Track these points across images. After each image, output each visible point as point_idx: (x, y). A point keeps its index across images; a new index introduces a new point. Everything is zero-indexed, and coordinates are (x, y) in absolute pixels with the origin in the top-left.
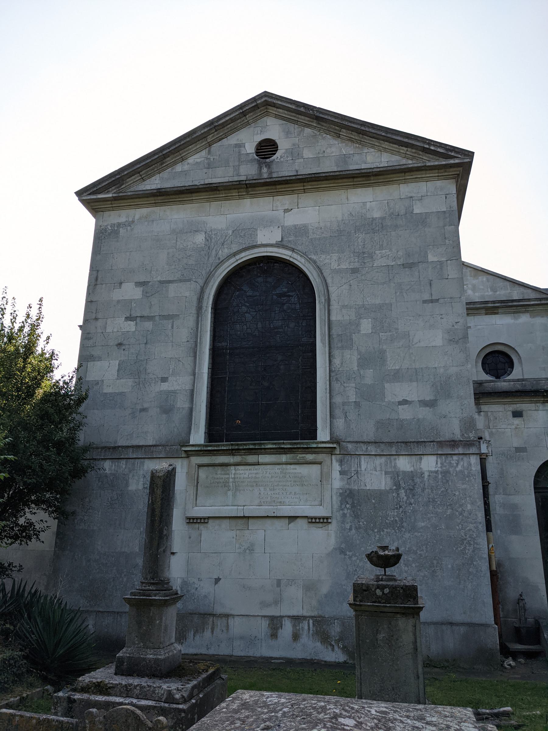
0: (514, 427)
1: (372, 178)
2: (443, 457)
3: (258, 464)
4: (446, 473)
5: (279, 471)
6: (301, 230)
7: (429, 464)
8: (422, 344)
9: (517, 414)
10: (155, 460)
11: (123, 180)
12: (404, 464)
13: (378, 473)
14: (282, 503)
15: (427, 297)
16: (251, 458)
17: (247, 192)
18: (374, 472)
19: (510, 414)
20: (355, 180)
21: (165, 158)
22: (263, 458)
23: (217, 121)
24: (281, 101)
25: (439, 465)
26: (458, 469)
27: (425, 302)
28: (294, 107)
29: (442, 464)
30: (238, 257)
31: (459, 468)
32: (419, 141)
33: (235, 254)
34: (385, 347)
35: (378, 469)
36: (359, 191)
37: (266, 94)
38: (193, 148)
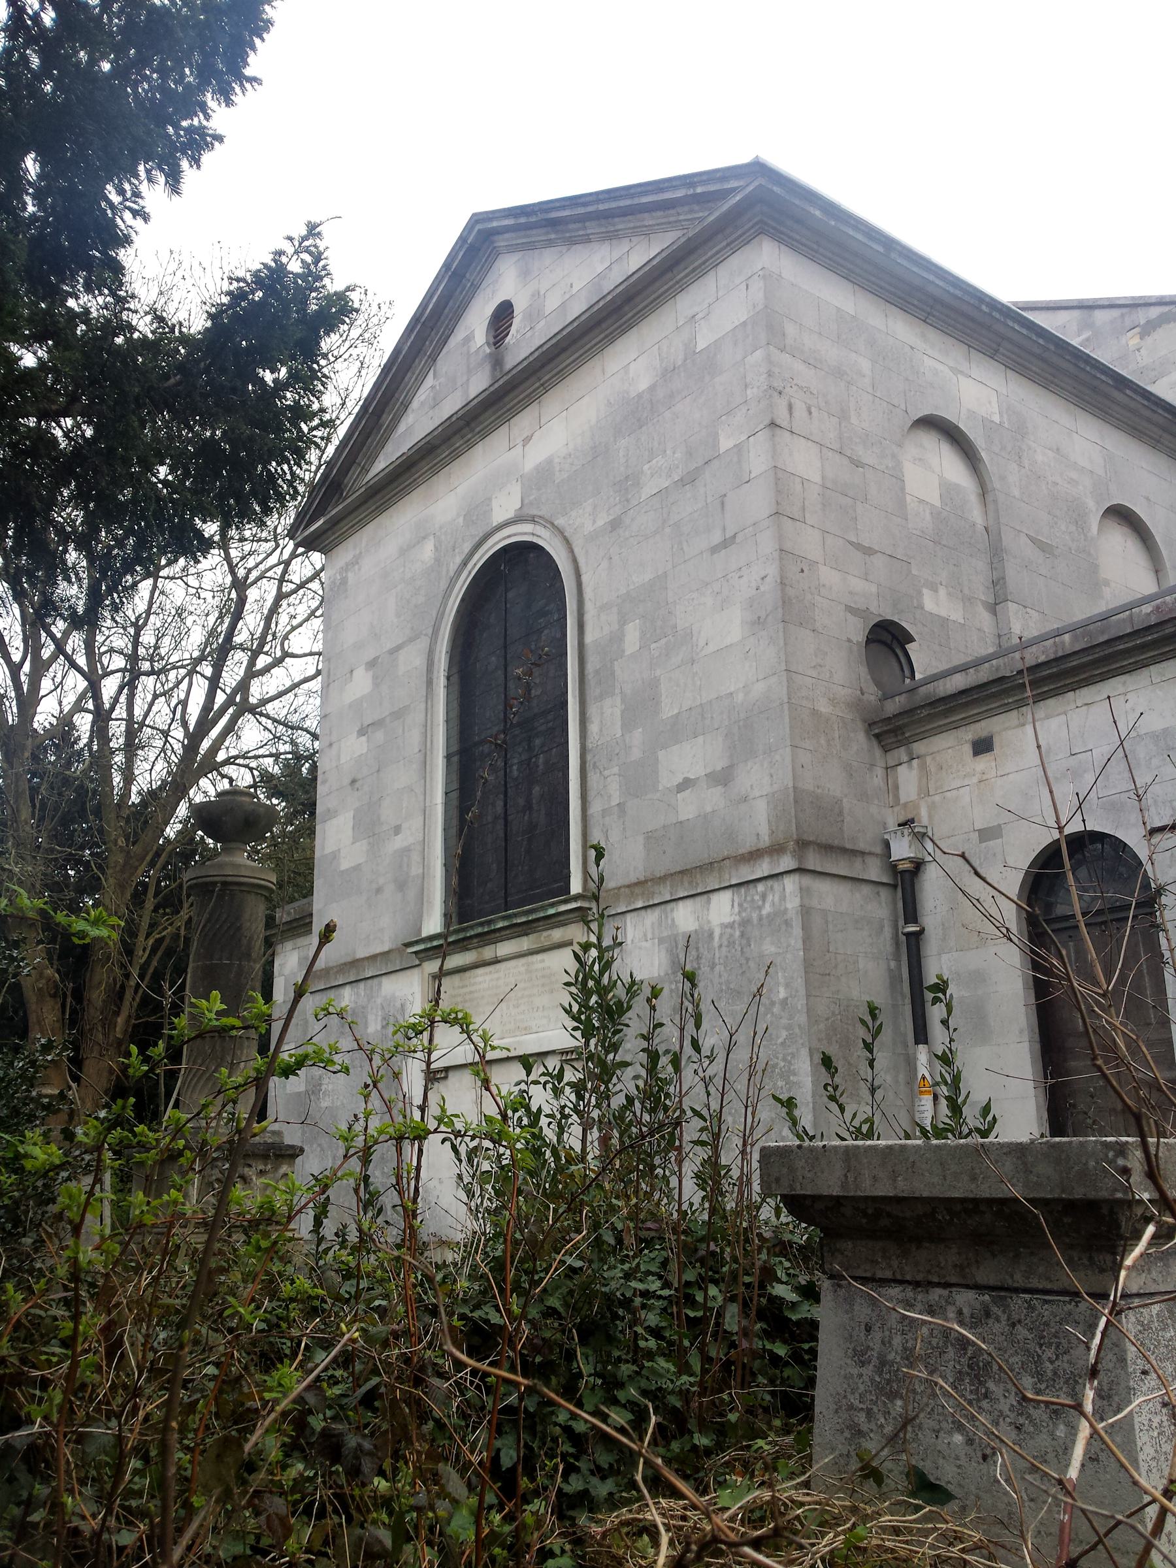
0: (975, 780)
1: (626, 308)
2: (743, 890)
3: (496, 961)
4: (745, 923)
5: (523, 969)
6: (544, 473)
7: (722, 909)
8: (712, 648)
9: (982, 747)
10: (408, 972)
11: (339, 485)
12: (685, 917)
13: (648, 944)
14: (528, 1030)
15: (717, 538)
16: (488, 953)
17: (472, 430)
18: (644, 944)
19: (968, 749)
20: (604, 326)
21: (379, 417)
22: (504, 948)
23: (422, 314)
24: (652, 192)
25: (736, 909)
26: (764, 912)
27: (714, 550)
28: (509, 222)
29: (740, 905)
30: (469, 566)
31: (767, 909)
32: (675, 188)
33: (465, 563)
34: (658, 673)
35: (649, 936)
36: (611, 351)
37: (477, 219)
38: (410, 378)
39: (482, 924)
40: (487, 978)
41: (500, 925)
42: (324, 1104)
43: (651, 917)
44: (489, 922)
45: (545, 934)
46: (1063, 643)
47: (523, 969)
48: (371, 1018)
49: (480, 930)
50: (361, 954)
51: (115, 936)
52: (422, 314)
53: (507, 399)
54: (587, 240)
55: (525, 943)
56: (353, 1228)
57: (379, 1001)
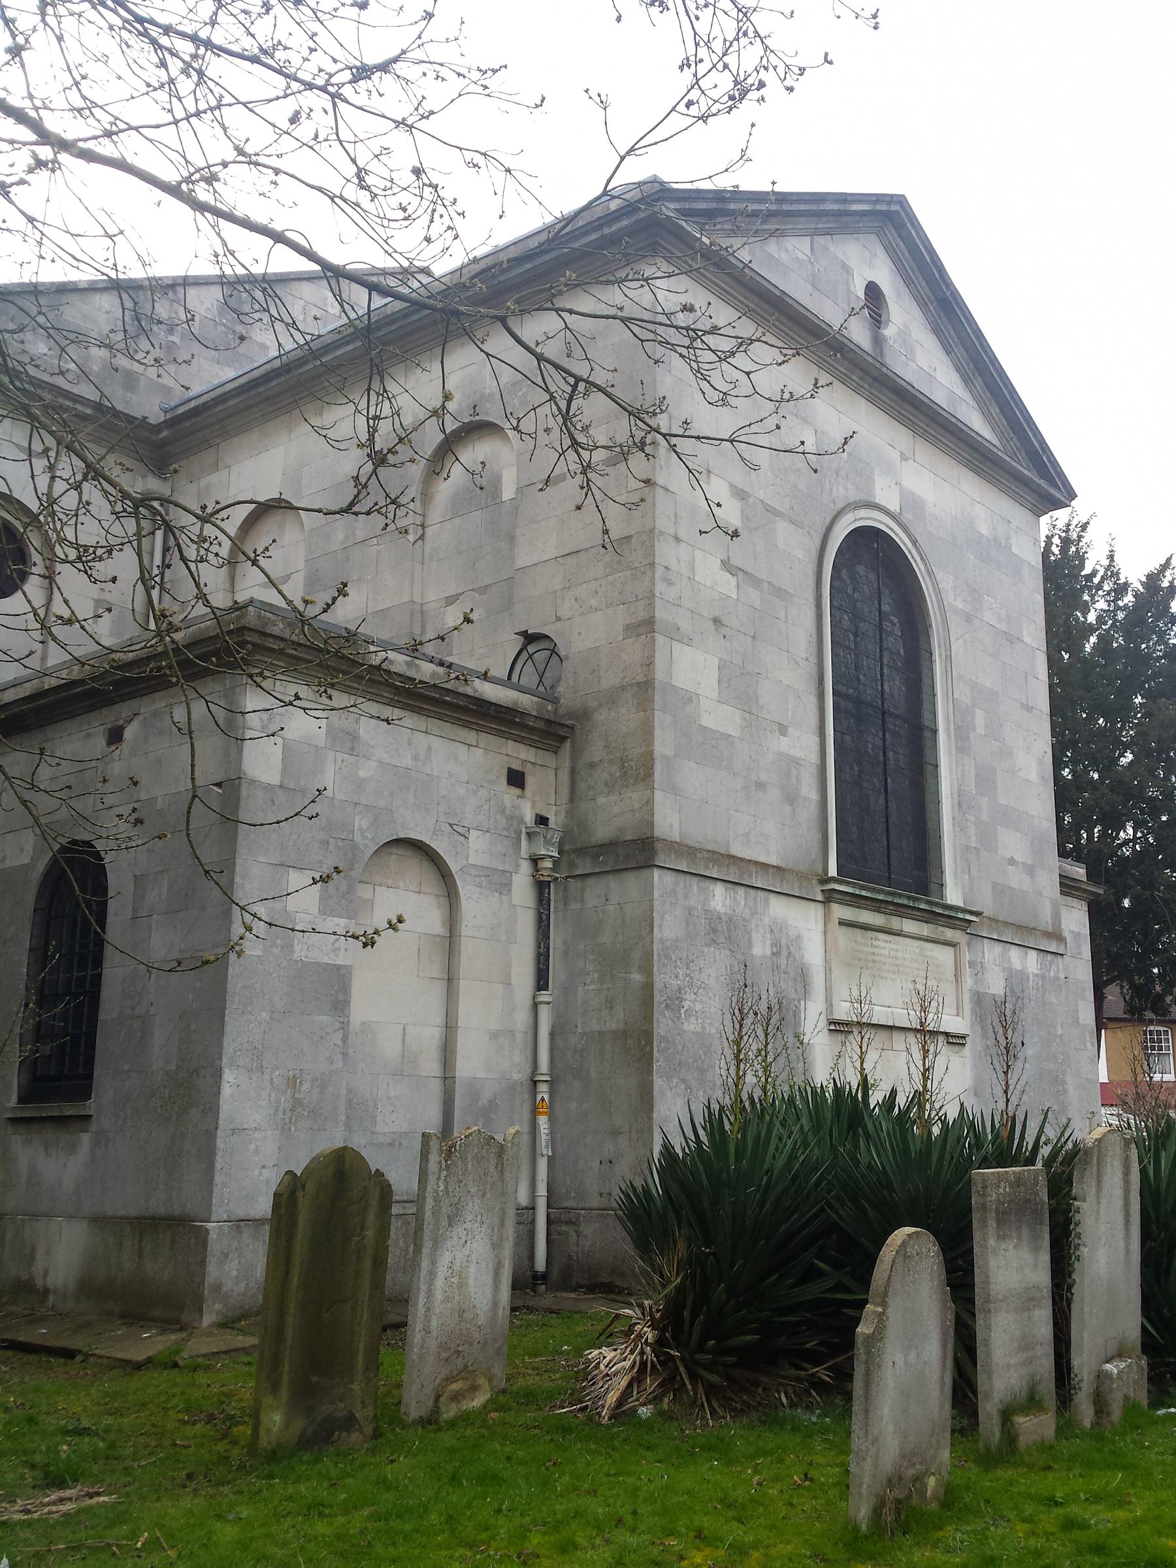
10: (804, 903)
16: (896, 923)
39: (909, 898)
40: (888, 945)
41: (922, 906)
42: (691, 1026)
43: (998, 948)
44: (915, 899)
45: (941, 929)
46: (800, 888)
47: (917, 951)
48: (756, 937)
49: (905, 902)
50: (737, 850)
51: (274, 353)
52: (994, 366)
53: (906, 406)
54: (857, 231)
55: (925, 929)
56: (180, 1416)
57: (767, 920)
